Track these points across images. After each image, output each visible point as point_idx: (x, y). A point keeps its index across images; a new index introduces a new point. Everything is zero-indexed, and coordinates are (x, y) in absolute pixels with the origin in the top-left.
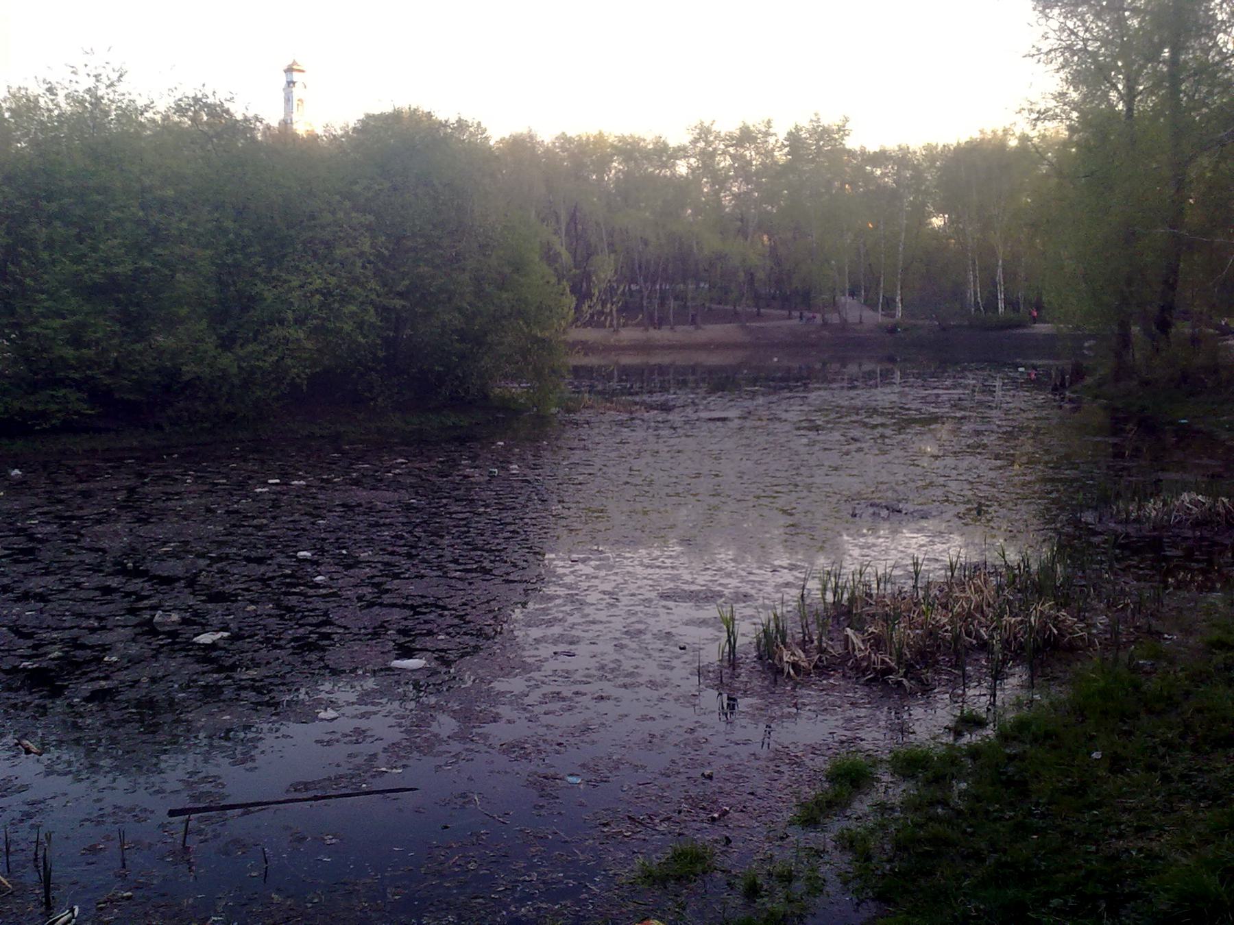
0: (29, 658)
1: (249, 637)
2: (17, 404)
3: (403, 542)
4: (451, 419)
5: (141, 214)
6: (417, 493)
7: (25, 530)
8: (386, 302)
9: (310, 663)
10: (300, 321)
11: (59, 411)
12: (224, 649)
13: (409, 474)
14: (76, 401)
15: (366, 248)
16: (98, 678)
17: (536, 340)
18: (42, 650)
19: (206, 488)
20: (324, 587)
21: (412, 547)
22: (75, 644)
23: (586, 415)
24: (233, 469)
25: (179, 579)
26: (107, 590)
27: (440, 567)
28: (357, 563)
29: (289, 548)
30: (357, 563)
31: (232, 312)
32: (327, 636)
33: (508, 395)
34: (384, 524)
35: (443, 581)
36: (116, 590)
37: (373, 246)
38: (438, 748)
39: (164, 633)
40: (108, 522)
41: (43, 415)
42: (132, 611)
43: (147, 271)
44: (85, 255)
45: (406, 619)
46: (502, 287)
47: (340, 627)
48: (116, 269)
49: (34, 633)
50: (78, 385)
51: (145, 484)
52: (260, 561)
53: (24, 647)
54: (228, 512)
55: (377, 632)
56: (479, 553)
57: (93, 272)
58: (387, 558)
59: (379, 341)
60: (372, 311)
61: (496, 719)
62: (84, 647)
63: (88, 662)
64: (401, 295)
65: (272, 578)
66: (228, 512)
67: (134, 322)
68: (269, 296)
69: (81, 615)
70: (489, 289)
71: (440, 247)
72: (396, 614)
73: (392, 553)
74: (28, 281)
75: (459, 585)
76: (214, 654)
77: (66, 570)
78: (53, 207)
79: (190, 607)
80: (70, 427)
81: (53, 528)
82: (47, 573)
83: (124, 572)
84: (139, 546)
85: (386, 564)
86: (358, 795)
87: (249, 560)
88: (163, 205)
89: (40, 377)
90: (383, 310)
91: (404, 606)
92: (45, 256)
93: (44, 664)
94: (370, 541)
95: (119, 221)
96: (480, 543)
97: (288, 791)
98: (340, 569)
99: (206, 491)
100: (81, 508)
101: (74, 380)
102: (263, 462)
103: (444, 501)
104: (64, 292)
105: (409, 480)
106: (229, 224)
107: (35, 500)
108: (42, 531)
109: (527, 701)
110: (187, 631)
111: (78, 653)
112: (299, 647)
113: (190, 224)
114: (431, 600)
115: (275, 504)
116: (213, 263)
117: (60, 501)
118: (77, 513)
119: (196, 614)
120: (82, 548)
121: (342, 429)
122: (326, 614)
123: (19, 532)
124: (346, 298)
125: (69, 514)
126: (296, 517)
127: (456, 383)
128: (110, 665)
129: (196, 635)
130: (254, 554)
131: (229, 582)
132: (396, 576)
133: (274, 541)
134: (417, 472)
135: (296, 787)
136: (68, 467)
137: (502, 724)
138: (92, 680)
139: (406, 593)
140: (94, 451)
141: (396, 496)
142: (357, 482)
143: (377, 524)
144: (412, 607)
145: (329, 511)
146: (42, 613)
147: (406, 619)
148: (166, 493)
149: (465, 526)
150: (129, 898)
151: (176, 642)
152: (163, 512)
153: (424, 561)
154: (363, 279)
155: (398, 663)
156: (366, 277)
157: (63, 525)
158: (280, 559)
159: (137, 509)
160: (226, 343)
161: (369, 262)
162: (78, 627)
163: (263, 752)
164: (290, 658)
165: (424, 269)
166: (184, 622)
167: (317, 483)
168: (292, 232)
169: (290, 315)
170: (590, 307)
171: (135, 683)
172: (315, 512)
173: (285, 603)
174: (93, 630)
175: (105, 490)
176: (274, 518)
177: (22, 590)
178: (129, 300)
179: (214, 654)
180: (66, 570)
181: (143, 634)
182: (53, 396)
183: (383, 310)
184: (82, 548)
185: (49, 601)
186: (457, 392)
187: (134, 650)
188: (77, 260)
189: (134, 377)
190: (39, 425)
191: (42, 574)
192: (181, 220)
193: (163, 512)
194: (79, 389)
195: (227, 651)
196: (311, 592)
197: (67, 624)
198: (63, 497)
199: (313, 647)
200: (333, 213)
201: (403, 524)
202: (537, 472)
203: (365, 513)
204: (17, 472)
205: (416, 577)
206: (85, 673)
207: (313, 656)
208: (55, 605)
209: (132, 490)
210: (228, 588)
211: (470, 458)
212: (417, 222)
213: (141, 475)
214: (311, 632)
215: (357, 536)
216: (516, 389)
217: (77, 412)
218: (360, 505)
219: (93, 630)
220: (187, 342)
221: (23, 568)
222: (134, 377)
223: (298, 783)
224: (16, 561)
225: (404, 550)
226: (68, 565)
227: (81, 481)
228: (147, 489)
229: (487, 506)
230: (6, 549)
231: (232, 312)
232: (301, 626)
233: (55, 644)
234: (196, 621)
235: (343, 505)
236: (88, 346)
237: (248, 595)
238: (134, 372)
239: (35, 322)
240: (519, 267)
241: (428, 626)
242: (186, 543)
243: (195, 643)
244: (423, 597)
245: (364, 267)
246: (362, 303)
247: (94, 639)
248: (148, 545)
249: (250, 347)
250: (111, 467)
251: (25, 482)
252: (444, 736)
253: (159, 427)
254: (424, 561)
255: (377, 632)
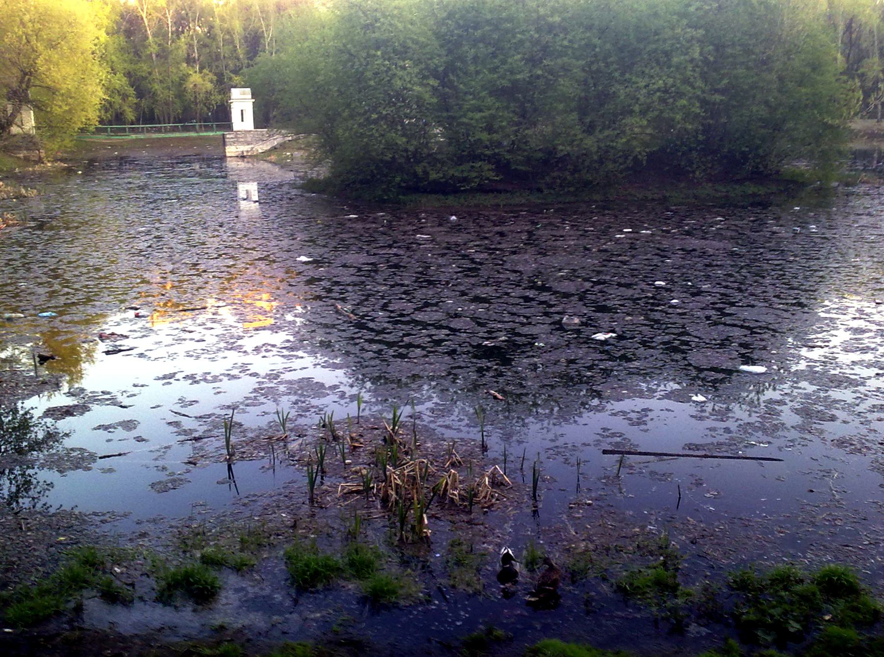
0: (487, 339)
1: (630, 338)
2: (451, 172)
3: (732, 279)
4: (751, 189)
5: (536, 36)
6: (737, 243)
7: (468, 256)
8: (707, 96)
9: (677, 361)
10: (643, 113)
12: (613, 345)
13: (728, 229)
14: (488, 171)
15: (696, 55)
16: (533, 356)
17: (827, 126)
18: (494, 335)
19: (581, 233)
20: (680, 308)
21: (741, 283)
22: (513, 332)
23: (863, 189)
24: (595, 221)
25: (573, 295)
26: (527, 299)
27: (765, 301)
28: (699, 293)
29: (648, 279)
30: (699, 293)
31: (595, 106)
32: (687, 343)
33: (797, 171)
34: (717, 266)
35: (771, 311)
36: (533, 299)
37: (701, 54)
38: (780, 433)
39: (572, 330)
40: (519, 253)
41: (465, 180)
42: (546, 314)
43: (538, 77)
44: (498, 67)
45: (746, 336)
46: (801, 84)
47: (696, 337)
48: (518, 77)
49: (487, 323)
51: (538, 229)
52: (628, 286)
53: (482, 332)
54: (599, 251)
55: (724, 343)
56: (796, 292)
57: (504, 79)
58: (723, 291)
59: (701, 128)
60: (698, 104)
61: (833, 418)
63: (524, 345)
64: (722, 92)
65: (640, 299)
66: (599, 251)
67: (526, 116)
68: (622, 93)
69: (513, 314)
70: (790, 85)
71: (753, 53)
72: (737, 332)
73: (726, 287)
74: (461, 86)
75: (785, 315)
76: (607, 348)
77: (498, 283)
79: (585, 314)
80: (482, 189)
81: (484, 256)
82: (488, 285)
83: (533, 287)
84: (543, 271)
85: (722, 294)
86: (734, 458)
87: (620, 285)
88: (551, 28)
90: (704, 103)
91: (742, 327)
92: (472, 68)
93: (498, 344)
94: (708, 277)
95: (521, 42)
96: (796, 284)
97: (684, 448)
98: (688, 295)
99: (581, 235)
100: (500, 243)
101: (485, 155)
102: (616, 216)
103: (762, 250)
104: (484, 94)
105: (729, 233)
106: (596, 41)
107: (470, 237)
108: (479, 257)
109: (858, 409)
110: (586, 331)
111: (517, 338)
112: (667, 349)
113: (570, 41)
114: (763, 324)
115: (633, 247)
116: (583, 70)
117: (486, 238)
118: (499, 246)
119: (590, 318)
120: (507, 270)
121: (668, 195)
122: (683, 327)
123: (464, 257)
124: (680, 95)
125: (493, 247)
126: (649, 256)
127: (759, 160)
128: (539, 348)
129: (595, 334)
130: (623, 281)
131: (609, 299)
132: (732, 304)
133: (636, 273)
134: (733, 228)
135: (690, 446)
137: (838, 423)
138: (528, 357)
139: (743, 317)
140: (498, 205)
141: (721, 245)
142: (688, 233)
143: (710, 265)
144: (748, 328)
145: (673, 253)
147: (746, 336)
148: (555, 236)
149: (781, 270)
150: (589, 505)
151: (580, 337)
152: (555, 249)
153: (752, 295)
154: (692, 80)
155: (744, 368)
156: (695, 78)
157: (491, 254)
158: (643, 286)
159: (536, 246)
160: (590, 129)
161: (697, 66)
162: (514, 322)
163: (652, 419)
164: (661, 356)
165: (741, 71)
166: (583, 324)
167: (660, 233)
168: (641, 46)
169: (637, 108)
170: (876, 99)
171: (556, 363)
172: (662, 254)
173: (652, 317)
174: (523, 324)
175: (512, 232)
176: (633, 256)
177: (473, 294)
178: (522, 99)
179: (607, 348)
180: (498, 283)
181: (557, 329)
182: (472, 167)
183: (704, 103)
184: (507, 270)
186: (757, 168)
187: (553, 340)
188: (494, 70)
189: (526, 153)
190: (464, 186)
191: (483, 286)
192: (563, 40)
193: (555, 249)
194: (489, 162)
195: (616, 347)
196: (670, 311)
198: (487, 235)
199: (676, 350)
200: (673, 29)
201: (732, 266)
202: (834, 231)
203: (700, 257)
204: (454, 218)
205: (748, 306)
206: (523, 352)
207: (678, 356)
208: (496, 306)
209: (530, 233)
210: (609, 304)
211: (775, 219)
212: (738, 34)
213: (534, 223)
214: (674, 339)
215: (697, 273)
216: (802, 166)
217: (488, 179)
218: (694, 250)
219: (523, 324)
220: (557, 129)
221: (473, 280)
222: (526, 153)
223: (690, 444)
224: (467, 276)
225: (736, 285)
228: (541, 232)
229: (796, 256)
231: (595, 106)
232: (667, 334)
234: (590, 323)
235: (682, 250)
237: (624, 309)
238: (525, 150)
239: (465, 116)
240: (816, 67)
241: (764, 343)
242: (575, 270)
243: (592, 339)
244: (757, 321)
245: (694, 71)
246: (690, 98)
247: (525, 330)
248: (549, 270)
249: (606, 133)
252: (788, 425)
253: (540, 190)
254: (752, 295)
255: (724, 343)
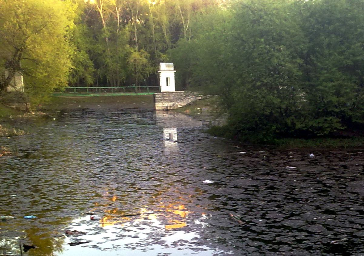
0: (334, 239)
2: (311, 123)
7: (321, 182)
11: (328, 127)
18: (338, 237)
22: (352, 235)
40: (357, 180)
41: (320, 129)
44: (344, 51)
50: (337, 115)
53: (330, 234)
57: (348, 59)
62: (356, 237)
63: (360, 244)
77: (342, 201)
78: (331, 28)
80: (332, 136)
82: (335, 202)
89: (321, 110)
92: (326, 52)
93: (341, 243)
100: (343, 173)
107: (323, 168)
108: (329, 182)
111: (354, 239)
118: (343, 175)
120: (348, 192)
125: (339, 175)
136: (333, 154)
146: (335, 220)
157: (337, 181)
162: (352, 228)
175: (352, 165)
177: (325, 208)
180: (342, 201)
182: (326, 120)
184: (348, 192)
185: (337, 215)
188: (341, 53)
190: (319, 133)
191: (332, 202)
194: (337, 117)
197: (347, 226)
198: (335, 167)
204: (312, 155)
208: (340, 216)
217: (336, 128)
221: (324, 199)
224: (321, 195)
226: (343, 199)
227: (341, 161)
230: (315, 189)
233: (343, 234)
236: (342, 96)
250: (353, 155)
251: (316, 160)
